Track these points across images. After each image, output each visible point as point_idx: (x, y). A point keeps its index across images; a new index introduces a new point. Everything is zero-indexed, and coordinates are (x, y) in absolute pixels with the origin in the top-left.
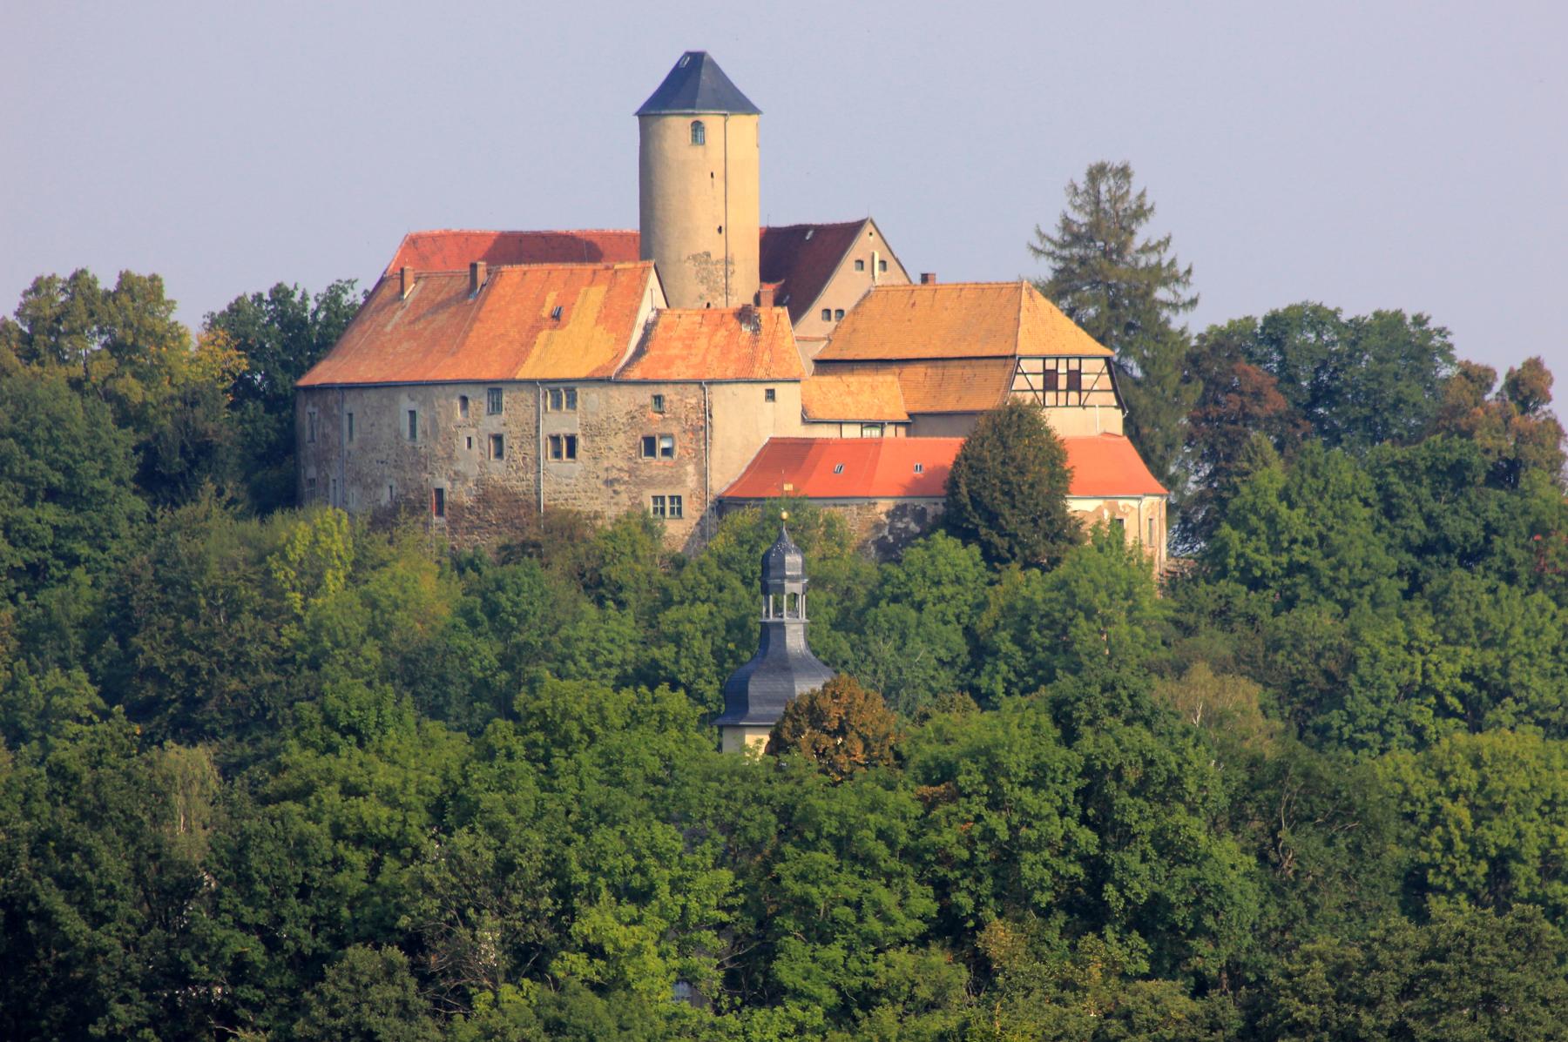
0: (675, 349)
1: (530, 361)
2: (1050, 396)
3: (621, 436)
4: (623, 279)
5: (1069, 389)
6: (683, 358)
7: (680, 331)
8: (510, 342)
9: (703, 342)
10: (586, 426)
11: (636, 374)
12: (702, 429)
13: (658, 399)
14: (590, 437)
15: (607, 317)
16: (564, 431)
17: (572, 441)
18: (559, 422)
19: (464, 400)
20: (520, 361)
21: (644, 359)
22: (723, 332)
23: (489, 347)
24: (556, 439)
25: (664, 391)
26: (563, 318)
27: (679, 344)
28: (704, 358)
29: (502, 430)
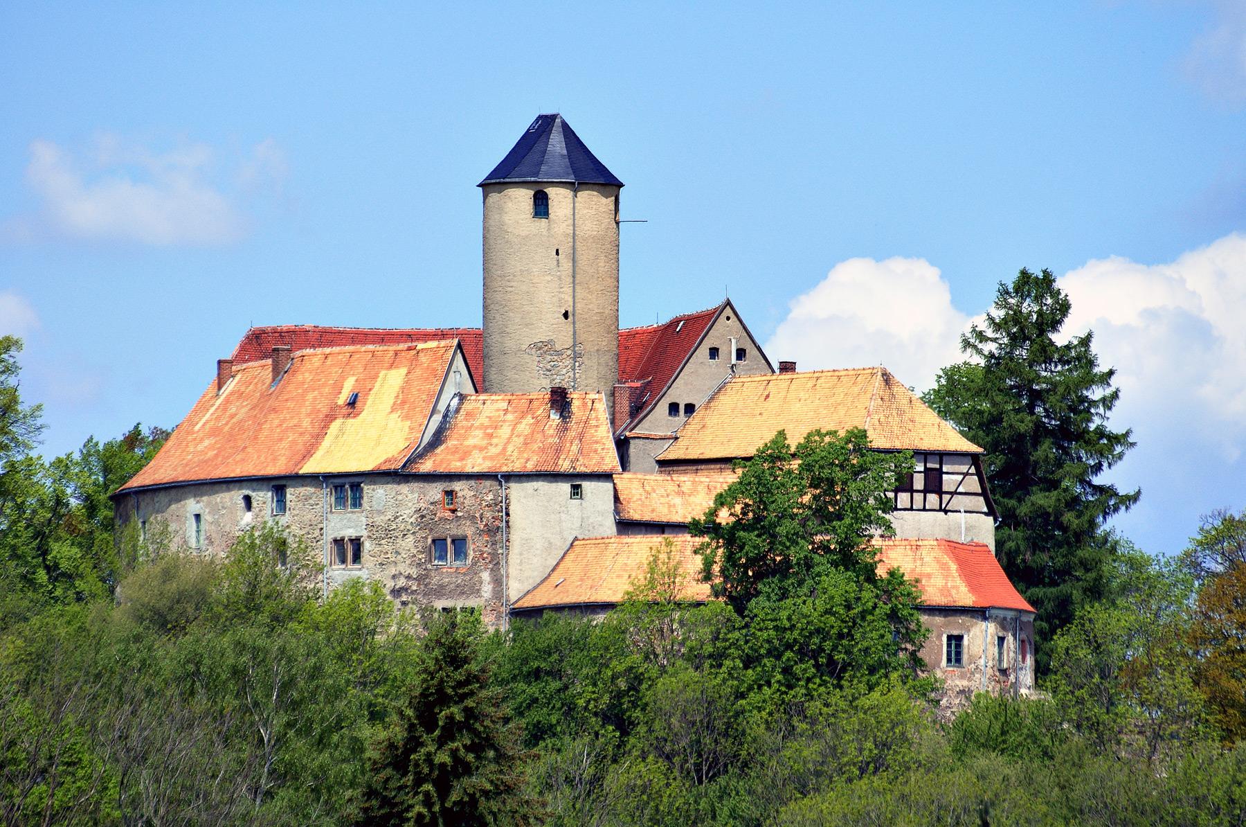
0: (476, 438)
1: (319, 454)
2: (904, 499)
3: (410, 538)
4: (423, 358)
5: (925, 491)
6: (481, 449)
7: (482, 420)
8: (301, 434)
9: (505, 431)
10: (371, 526)
11: (426, 466)
12: (498, 528)
13: (450, 494)
14: (377, 540)
15: (404, 402)
16: (350, 533)
17: (357, 543)
18: (347, 524)
19: (248, 500)
20: (308, 454)
21: (439, 450)
22: (529, 420)
23: (281, 440)
24: (339, 542)
25: (457, 486)
26: (358, 404)
27: (479, 433)
28: (504, 449)
29: (200, 512)
